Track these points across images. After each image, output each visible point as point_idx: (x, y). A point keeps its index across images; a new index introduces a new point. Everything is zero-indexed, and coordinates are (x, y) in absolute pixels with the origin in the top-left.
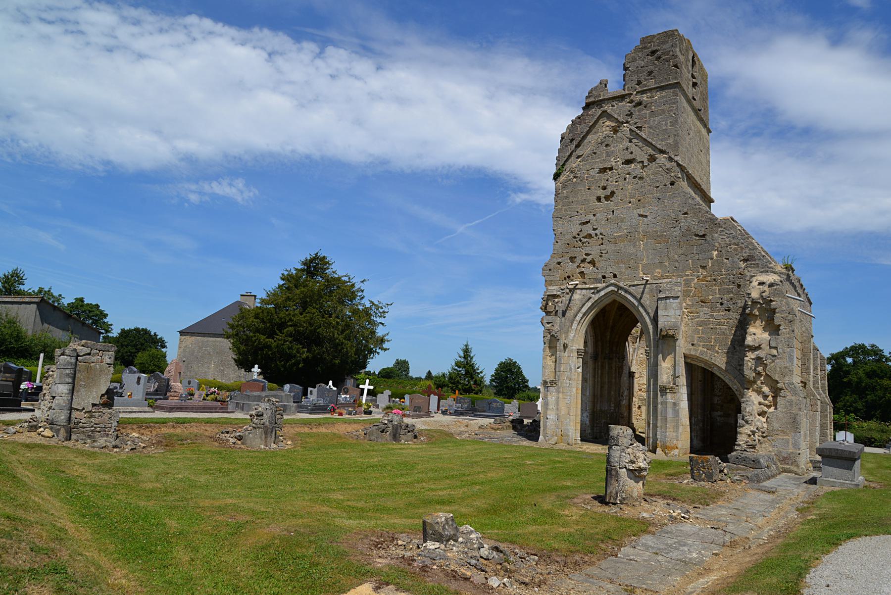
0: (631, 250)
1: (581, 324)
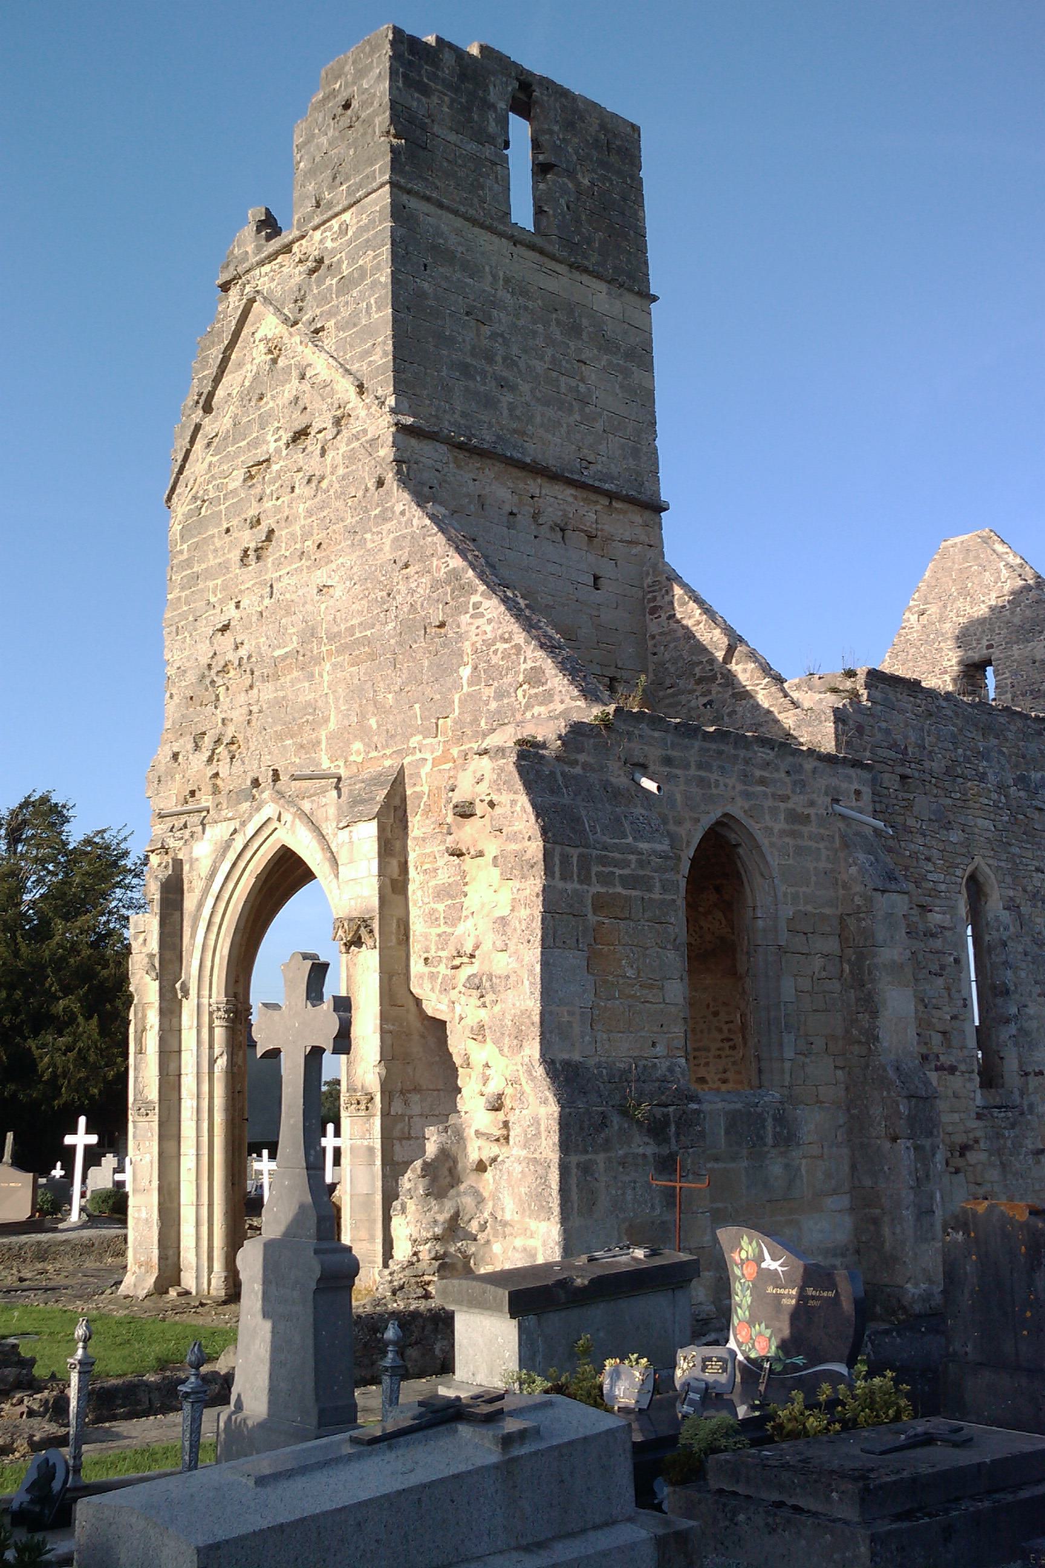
1: (215, 929)
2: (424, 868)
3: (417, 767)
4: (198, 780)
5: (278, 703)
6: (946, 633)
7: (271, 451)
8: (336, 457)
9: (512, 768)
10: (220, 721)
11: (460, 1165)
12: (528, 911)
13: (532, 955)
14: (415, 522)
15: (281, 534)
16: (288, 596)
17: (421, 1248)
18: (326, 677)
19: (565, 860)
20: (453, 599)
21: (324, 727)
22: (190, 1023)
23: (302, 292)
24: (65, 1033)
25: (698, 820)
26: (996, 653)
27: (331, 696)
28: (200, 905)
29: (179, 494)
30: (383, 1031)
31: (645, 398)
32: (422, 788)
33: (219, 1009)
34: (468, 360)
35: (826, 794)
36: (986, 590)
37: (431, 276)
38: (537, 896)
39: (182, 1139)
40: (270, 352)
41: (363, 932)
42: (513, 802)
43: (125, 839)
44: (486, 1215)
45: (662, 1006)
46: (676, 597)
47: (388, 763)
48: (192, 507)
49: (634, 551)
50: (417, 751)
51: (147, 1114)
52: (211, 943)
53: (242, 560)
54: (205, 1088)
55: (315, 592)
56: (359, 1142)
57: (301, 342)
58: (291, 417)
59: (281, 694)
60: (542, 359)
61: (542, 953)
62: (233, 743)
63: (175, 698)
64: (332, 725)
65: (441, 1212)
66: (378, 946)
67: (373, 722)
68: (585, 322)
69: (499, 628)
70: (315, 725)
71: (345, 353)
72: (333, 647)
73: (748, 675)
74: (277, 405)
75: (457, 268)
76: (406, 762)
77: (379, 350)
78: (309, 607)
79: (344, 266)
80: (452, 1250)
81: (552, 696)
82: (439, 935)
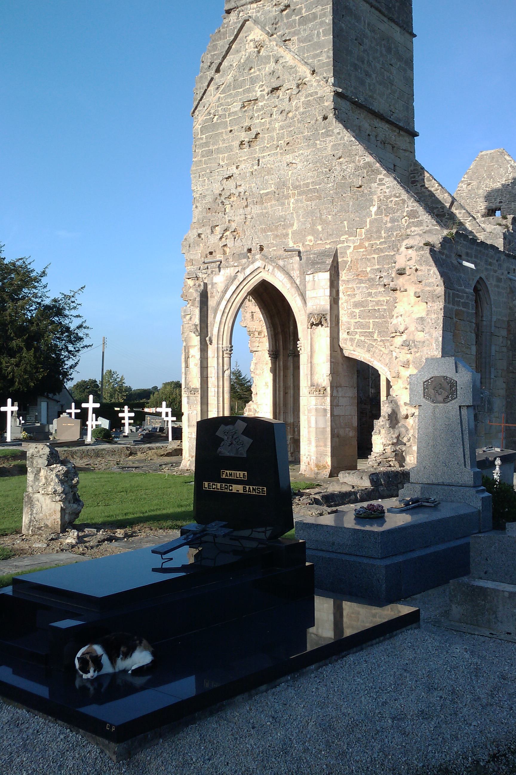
0: (280, 212)
1: (226, 315)
2: (347, 294)
3: (345, 249)
4: (214, 247)
5: (263, 215)
6: (480, 194)
7: (258, 95)
8: (299, 103)
9: (428, 255)
10: (227, 221)
11: (398, 416)
12: (436, 316)
13: (438, 334)
14: (346, 138)
15: (265, 136)
16: (269, 166)
17: (387, 448)
18: (291, 205)
19: (449, 294)
20: (367, 176)
21: (290, 228)
22: (213, 355)
23: (277, 20)
24: (16, 357)
25: (473, 279)
26: (503, 206)
27: (295, 215)
28: (219, 304)
29: (199, 111)
30: (331, 362)
31: (409, 82)
32: (347, 259)
33: (227, 350)
34: (356, 62)
35: (506, 270)
36: (500, 177)
37: (344, 21)
38: (441, 309)
39: (209, 405)
40: (257, 47)
41: (323, 319)
42: (429, 270)
43: (30, 264)
44: (410, 435)
45: (470, 356)
46: (426, 177)
47: (328, 246)
48: (208, 117)
49: (406, 154)
50: (345, 242)
51: (195, 394)
52: (224, 321)
53: (240, 146)
54: (221, 383)
55: (286, 165)
56: (319, 407)
57: (276, 45)
58: (270, 81)
59: (264, 211)
60: (379, 63)
61: (443, 333)
62: (234, 231)
63: (199, 208)
64: (295, 227)
65: (394, 434)
66: (329, 326)
67: (319, 228)
68: (393, 46)
69: (393, 191)
70: (285, 227)
71: (304, 54)
72: (296, 192)
73: (461, 215)
74: (262, 74)
75: (353, 17)
76: (338, 246)
77: (324, 55)
78: (282, 172)
79: (304, 11)
80: (397, 448)
81: (422, 223)
82: (356, 323)
